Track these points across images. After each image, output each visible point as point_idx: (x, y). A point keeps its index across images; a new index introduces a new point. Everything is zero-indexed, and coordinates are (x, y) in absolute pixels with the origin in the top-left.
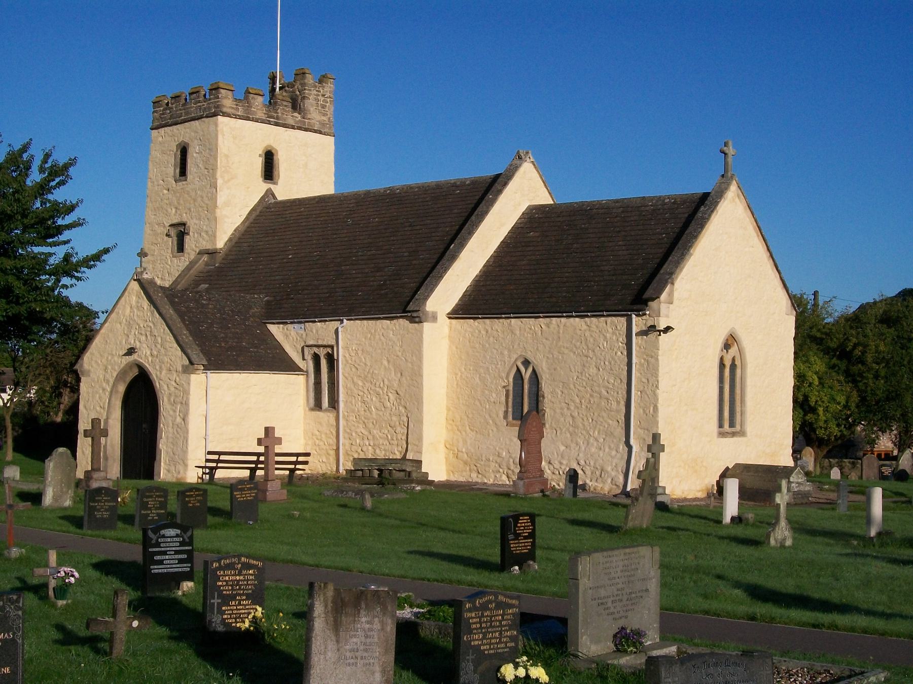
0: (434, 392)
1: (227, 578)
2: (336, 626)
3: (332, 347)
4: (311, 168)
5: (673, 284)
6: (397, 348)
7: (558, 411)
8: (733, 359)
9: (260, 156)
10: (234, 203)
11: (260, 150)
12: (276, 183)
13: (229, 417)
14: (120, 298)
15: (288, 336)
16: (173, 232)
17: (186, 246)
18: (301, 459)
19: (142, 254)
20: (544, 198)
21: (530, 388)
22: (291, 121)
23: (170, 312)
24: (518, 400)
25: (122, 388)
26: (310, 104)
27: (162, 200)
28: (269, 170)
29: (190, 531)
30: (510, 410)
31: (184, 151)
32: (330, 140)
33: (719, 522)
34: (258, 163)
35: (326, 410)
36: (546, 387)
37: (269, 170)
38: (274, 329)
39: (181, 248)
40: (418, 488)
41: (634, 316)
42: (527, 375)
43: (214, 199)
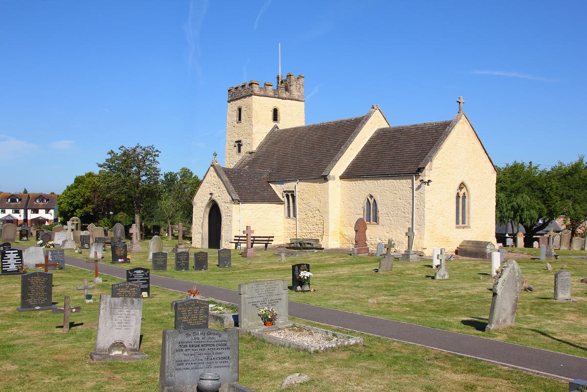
1: (122, 292)
2: (112, 313)
3: (293, 191)
4: (294, 115)
8: (464, 194)
9: (271, 111)
10: (258, 131)
14: (207, 173)
15: (278, 189)
16: (236, 144)
17: (241, 150)
18: (270, 239)
19: (215, 155)
20: (385, 125)
21: (373, 208)
22: (284, 96)
23: (226, 178)
24: (369, 213)
25: (208, 210)
28: (275, 117)
29: (148, 271)
31: (240, 110)
32: (303, 104)
33: (432, 267)
34: (271, 115)
36: (379, 207)
37: (275, 117)
38: (271, 185)
39: (239, 151)
43: (251, 130)
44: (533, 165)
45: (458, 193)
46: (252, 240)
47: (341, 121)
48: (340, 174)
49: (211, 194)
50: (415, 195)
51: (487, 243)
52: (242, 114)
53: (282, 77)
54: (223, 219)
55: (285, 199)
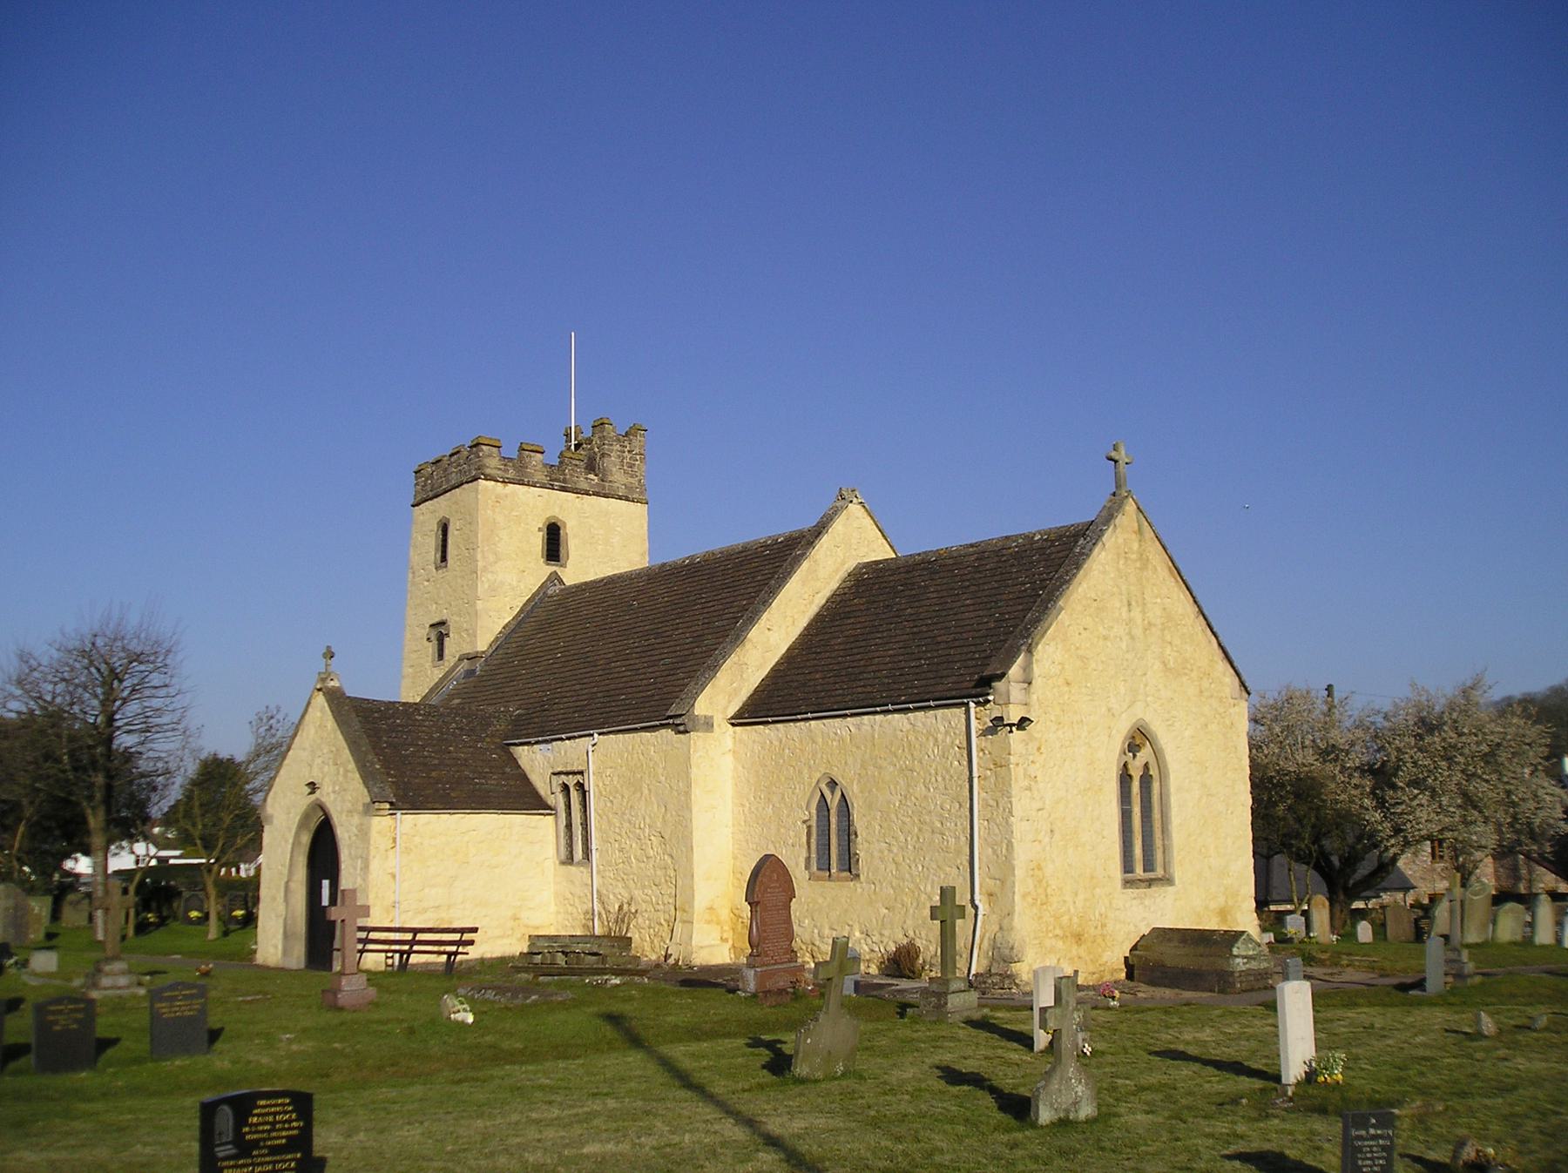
0: (692, 827)
3: (581, 773)
4: (613, 540)
5: (1030, 651)
6: (660, 771)
7: (876, 854)
8: (1146, 766)
11: (541, 523)
12: (564, 566)
13: (469, 882)
15: (538, 761)
17: (446, 652)
18: (467, 937)
20: (881, 551)
21: (839, 822)
22: (584, 485)
23: (356, 723)
25: (306, 839)
26: (612, 464)
27: (427, 596)
30: (814, 855)
31: (444, 529)
32: (641, 509)
34: (538, 542)
35: (579, 863)
39: (441, 656)
40: (617, 981)
41: (972, 705)
42: (834, 802)
44: (1336, 694)
45: (1125, 765)
46: (360, 941)
47: (745, 549)
48: (733, 709)
49: (313, 787)
50: (975, 774)
51: (1233, 937)
52: (450, 541)
53: (579, 431)
54: (343, 866)
55: (558, 800)
